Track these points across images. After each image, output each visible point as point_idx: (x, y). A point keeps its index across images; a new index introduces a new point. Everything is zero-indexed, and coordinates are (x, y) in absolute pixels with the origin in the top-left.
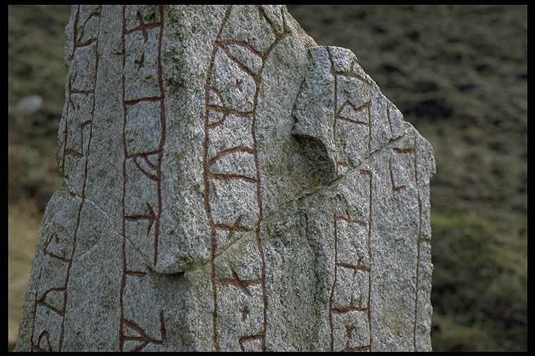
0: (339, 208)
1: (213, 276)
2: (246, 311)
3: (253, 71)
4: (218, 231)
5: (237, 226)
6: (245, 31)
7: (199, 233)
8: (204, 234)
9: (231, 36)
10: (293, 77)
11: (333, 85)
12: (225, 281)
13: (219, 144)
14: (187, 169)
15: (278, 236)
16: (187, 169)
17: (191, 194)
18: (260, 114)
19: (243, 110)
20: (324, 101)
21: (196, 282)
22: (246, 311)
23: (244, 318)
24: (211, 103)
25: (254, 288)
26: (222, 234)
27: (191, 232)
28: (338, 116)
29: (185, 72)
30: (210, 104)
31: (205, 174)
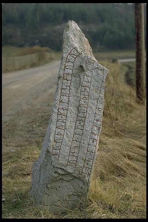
2: (67, 83)
12: (65, 80)
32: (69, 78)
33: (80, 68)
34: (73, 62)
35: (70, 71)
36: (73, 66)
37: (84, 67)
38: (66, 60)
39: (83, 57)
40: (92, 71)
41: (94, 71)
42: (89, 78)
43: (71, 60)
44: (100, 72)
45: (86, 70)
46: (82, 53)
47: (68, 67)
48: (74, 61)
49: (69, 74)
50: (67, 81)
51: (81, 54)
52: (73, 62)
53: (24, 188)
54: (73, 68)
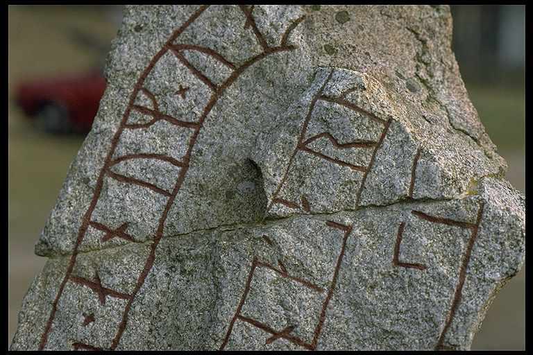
0: (264, 253)
1: (70, 270)
2: (90, 318)
3: (213, 81)
4: (90, 228)
5: (122, 231)
6: (213, 37)
7: (66, 222)
8: (72, 226)
9: (192, 41)
10: (276, 96)
11: (307, 110)
12: (81, 280)
13: (133, 146)
14: (82, 161)
15: (179, 261)
16: (82, 161)
17: (79, 185)
18: (208, 129)
19: (184, 119)
20: (289, 126)
21: (49, 269)
22: (90, 318)
23: (86, 323)
24: (137, 103)
25: (113, 299)
26: (94, 234)
27: (58, 219)
28: (302, 146)
29: (111, 68)
30: (135, 104)
31: (103, 171)
32: (124, 267)
33: (242, 186)
34: (187, 124)
35: (142, 208)
36: (185, 164)
37: (274, 175)
38: (134, 97)
39: (298, 77)
40: (348, 229)
41: (370, 228)
42: (306, 295)
43: (179, 101)
44: (426, 241)
45: (283, 209)
46: (296, 37)
47: (133, 168)
48: (199, 112)
49: (130, 232)
50: (93, 300)
51: (287, 46)
52: (187, 124)
53: (89, 164)
54: (182, 174)
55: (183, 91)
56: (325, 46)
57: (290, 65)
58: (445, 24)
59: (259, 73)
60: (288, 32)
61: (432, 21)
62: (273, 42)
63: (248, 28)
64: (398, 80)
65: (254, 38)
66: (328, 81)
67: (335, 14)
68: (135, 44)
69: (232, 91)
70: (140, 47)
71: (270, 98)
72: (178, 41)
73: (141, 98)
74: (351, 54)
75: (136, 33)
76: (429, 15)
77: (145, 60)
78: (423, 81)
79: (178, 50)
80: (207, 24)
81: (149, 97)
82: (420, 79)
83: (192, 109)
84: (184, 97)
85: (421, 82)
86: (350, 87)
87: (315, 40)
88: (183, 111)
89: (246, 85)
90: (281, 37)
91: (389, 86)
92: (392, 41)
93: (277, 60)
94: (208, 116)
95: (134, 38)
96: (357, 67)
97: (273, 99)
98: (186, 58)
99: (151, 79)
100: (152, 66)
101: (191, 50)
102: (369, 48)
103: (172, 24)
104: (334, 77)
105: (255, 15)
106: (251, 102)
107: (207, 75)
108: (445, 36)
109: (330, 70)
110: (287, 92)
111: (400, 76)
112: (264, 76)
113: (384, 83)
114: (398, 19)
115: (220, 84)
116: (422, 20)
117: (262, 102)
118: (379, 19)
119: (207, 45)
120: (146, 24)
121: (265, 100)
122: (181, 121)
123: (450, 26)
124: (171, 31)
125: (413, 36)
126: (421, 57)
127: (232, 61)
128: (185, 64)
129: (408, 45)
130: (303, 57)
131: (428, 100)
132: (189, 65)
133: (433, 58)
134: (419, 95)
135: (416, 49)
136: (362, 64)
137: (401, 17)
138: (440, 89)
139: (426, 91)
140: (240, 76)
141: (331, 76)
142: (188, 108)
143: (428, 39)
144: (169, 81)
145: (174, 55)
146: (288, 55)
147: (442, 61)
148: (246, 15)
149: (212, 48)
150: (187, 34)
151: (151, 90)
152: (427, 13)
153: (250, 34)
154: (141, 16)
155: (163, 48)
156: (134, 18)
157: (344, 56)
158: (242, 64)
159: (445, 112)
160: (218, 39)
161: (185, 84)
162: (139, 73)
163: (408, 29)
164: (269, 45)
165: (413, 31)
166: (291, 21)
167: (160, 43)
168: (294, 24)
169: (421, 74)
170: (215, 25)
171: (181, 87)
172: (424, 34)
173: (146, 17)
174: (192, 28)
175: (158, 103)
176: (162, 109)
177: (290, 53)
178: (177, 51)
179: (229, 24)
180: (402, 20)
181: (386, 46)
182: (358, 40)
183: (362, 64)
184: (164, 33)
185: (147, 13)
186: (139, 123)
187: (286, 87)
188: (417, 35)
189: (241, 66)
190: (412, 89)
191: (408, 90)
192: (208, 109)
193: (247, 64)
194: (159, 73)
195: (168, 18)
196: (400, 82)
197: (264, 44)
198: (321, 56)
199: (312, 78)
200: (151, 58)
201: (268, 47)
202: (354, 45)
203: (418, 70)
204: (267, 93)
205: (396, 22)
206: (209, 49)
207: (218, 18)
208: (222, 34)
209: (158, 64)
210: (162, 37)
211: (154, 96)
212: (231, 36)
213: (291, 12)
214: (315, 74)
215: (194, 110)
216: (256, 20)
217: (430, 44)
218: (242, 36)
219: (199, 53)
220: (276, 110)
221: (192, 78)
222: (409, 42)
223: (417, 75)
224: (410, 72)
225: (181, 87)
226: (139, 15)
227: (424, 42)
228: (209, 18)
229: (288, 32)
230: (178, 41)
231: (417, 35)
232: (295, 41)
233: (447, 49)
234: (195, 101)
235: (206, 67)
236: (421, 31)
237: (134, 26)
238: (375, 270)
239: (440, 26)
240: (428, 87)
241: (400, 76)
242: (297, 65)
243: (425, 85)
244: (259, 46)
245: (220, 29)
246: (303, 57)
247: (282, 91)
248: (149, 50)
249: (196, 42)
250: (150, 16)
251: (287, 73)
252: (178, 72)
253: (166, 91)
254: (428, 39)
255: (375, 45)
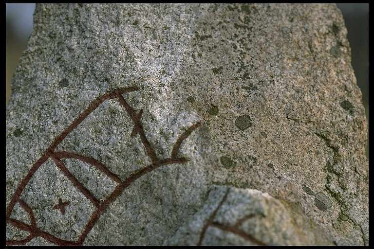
3: (96, 195)
6: (97, 146)
43: (57, 217)
46: (189, 148)
51: (178, 158)
55: (62, 206)
56: (221, 158)
57: (180, 180)
58: (360, 128)
59: (146, 188)
60: (180, 142)
61: (345, 125)
62: (162, 153)
63: (135, 136)
64: (305, 198)
65: (141, 148)
66: (221, 203)
67: (235, 119)
68: (14, 150)
69: (116, 207)
70: (19, 153)
71: (157, 218)
72: (60, 148)
73: (18, 212)
74: (251, 167)
75: (16, 138)
76: (341, 119)
77: (23, 168)
78: (335, 195)
79: (59, 158)
80: (91, 130)
81: (26, 210)
82: (331, 192)
83: (71, 226)
84: (63, 212)
85: (332, 196)
86: (248, 213)
87: (210, 151)
88: (62, 228)
89: (132, 201)
90: (172, 147)
91: (294, 206)
92: (299, 150)
93: (166, 174)
94: (89, 235)
95: (14, 143)
96: (258, 183)
97: (161, 219)
98: (68, 167)
99: (29, 190)
100: (30, 175)
101: (73, 159)
102: (273, 158)
103: (54, 128)
104: (229, 199)
105: (144, 121)
106: (136, 221)
107: (89, 189)
108: (360, 142)
109: (225, 190)
110: (176, 212)
111: (308, 191)
112: (151, 192)
113: (289, 202)
114: (306, 124)
115: (103, 199)
116: (334, 125)
117: (148, 222)
118: (285, 124)
119: (89, 154)
120: (26, 128)
121: (153, 219)
122: (60, 240)
123: (365, 129)
124: (52, 137)
125: (324, 142)
126: (332, 167)
127: (117, 173)
128: (66, 174)
129: (317, 153)
130: (196, 171)
131: (340, 218)
132: (70, 175)
133: (346, 168)
134: (330, 214)
135: (327, 157)
136: (264, 180)
137: (310, 122)
138: (353, 204)
139: (338, 207)
140: (125, 191)
141: (225, 198)
142: (67, 224)
143: (340, 145)
144: (48, 194)
145: (55, 165)
146: (178, 168)
147: (356, 171)
148: (134, 120)
149: (96, 157)
150: (69, 140)
151: (29, 202)
152: (340, 116)
153: (138, 143)
154: (22, 119)
155: (43, 156)
156: (14, 121)
157: (244, 169)
158: (128, 176)
159: (359, 232)
160: (102, 148)
161: (65, 198)
162: (16, 183)
163: (318, 135)
164: (158, 157)
165: (323, 137)
166: (183, 129)
167: (41, 149)
168: (187, 132)
169: (333, 186)
170: (100, 132)
171: (60, 200)
172: (336, 139)
173: (27, 120)
174: (75, 134)
175: (36, 217)
176: (39, 224)
177: (181, 166)
178: (58, 159)
179: (115, 131)
180: (311, 125)
181: (293, 155)
182: (260, 150)
183: (264, 180)
184: (45, 138)
185: (28, 115)
186: (15, 239)
187: (175, 206)
188: (328, 141)
189: (126, 179)
190: (322, 206)
191: (316, 209)
192: (89, 227)
193: (134, 177)
194: (37, 183)
195: (50, 122)
196: (307, 199)
197: (151, 153)
198: (216, 169)
199: (205, 197)
200: (30, 166)
201: (157, 159)
202: (255, 156)
203: (328, 182)
204: (154, 211)
205: (304, 128)
206: (92, 158)
207: (103, 124)
208: (106, 142)
209: (37, 174)
210: (42, 143)
211: (31, 209)
212: (117, 145)
213: (184, 118)
214: (209, 191)
215: (74, 228)
216: (145, 127)
217: (343, 151)
218: (128, 145)
219: (81, 163)
220: (164, 231)
221: (73, 191)
222: (318, 149)
223: (327, 188)
224: (320, 185)
225: (60, 200)
226: (19, 118)
227: (336, 149)
228: (93, 123)
229: (180, 142)
230: (60, 148)
231: (328, 141)
232: (188, 152)
233: (362, 156)
234: (75, 217)
235: (88, 179)
236: (333, 137)
237: (14, 129)
238: (307, 53)
239: (355, 130)
240: (340, 202)
241: (308, 191)
242: (189, 181)
243: (337, 199)
244: (147, 157)
245: (104, 137)
246: (196, 171)
247: (171, 210)
248: (28, 158)
249: (78, 150)
250: (31, 119)
251: (177, 190)
252: (59, 183)
253: (44, 204)
254: (340, 145)
255: (279, 154)
